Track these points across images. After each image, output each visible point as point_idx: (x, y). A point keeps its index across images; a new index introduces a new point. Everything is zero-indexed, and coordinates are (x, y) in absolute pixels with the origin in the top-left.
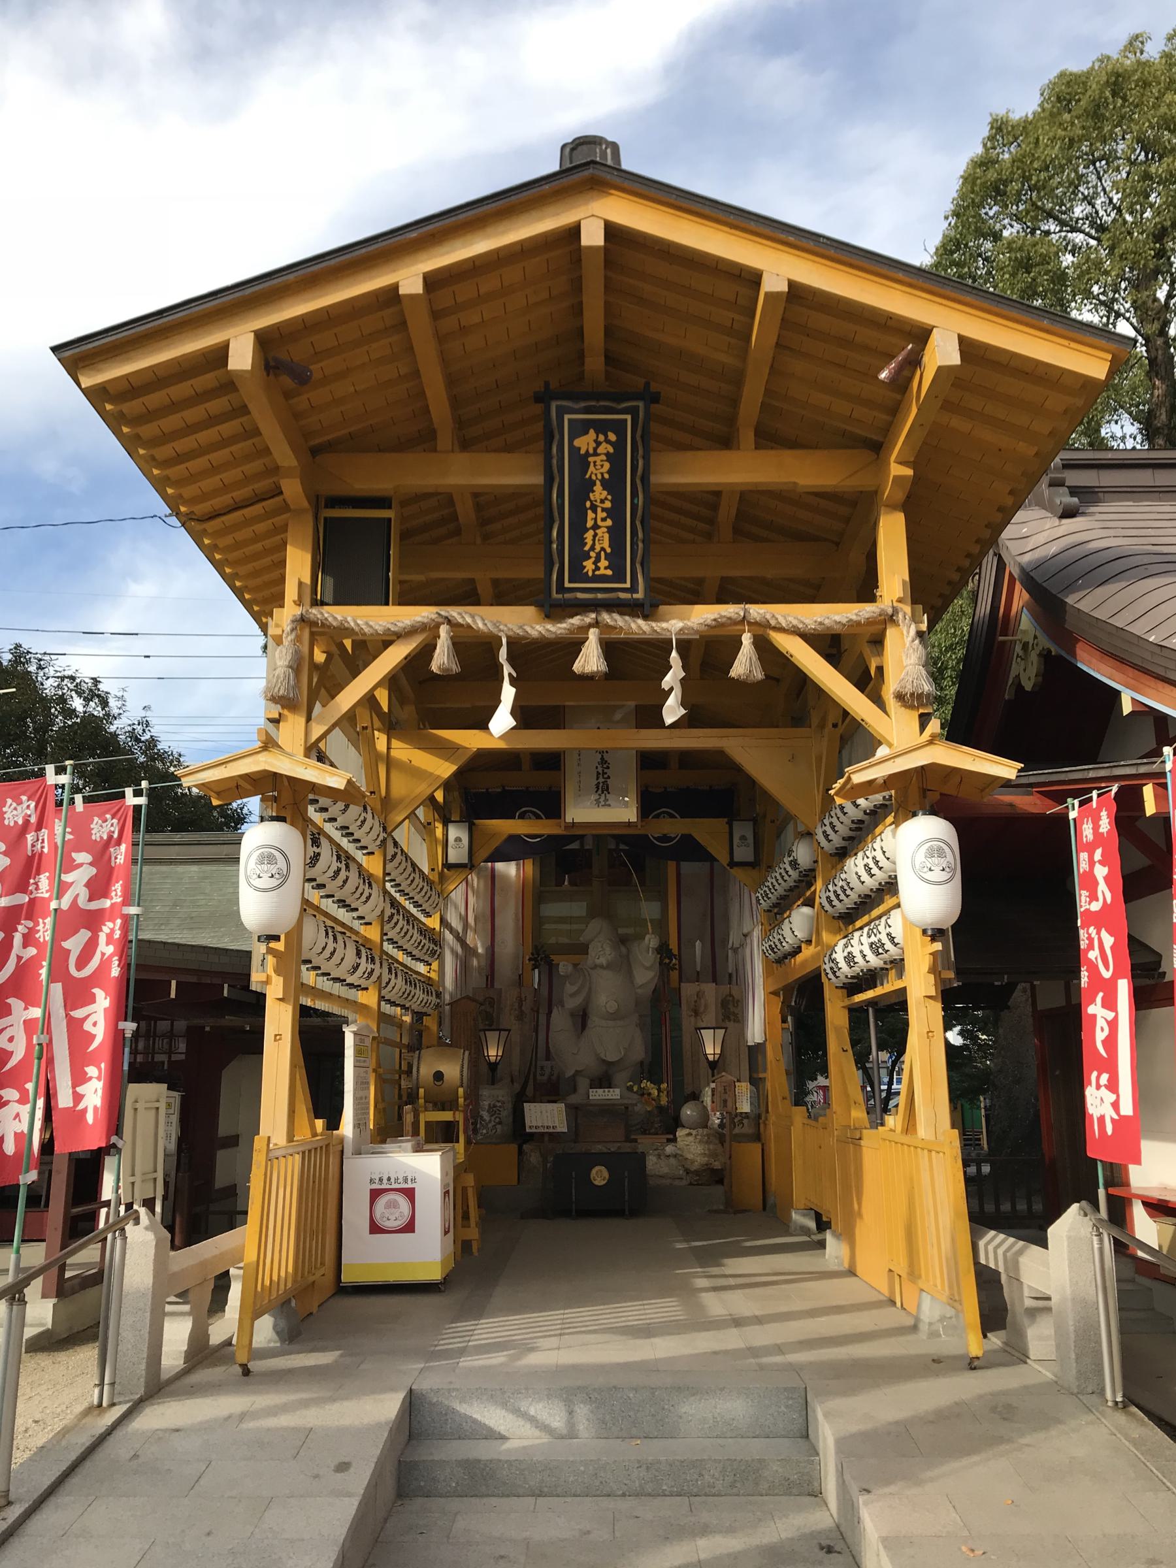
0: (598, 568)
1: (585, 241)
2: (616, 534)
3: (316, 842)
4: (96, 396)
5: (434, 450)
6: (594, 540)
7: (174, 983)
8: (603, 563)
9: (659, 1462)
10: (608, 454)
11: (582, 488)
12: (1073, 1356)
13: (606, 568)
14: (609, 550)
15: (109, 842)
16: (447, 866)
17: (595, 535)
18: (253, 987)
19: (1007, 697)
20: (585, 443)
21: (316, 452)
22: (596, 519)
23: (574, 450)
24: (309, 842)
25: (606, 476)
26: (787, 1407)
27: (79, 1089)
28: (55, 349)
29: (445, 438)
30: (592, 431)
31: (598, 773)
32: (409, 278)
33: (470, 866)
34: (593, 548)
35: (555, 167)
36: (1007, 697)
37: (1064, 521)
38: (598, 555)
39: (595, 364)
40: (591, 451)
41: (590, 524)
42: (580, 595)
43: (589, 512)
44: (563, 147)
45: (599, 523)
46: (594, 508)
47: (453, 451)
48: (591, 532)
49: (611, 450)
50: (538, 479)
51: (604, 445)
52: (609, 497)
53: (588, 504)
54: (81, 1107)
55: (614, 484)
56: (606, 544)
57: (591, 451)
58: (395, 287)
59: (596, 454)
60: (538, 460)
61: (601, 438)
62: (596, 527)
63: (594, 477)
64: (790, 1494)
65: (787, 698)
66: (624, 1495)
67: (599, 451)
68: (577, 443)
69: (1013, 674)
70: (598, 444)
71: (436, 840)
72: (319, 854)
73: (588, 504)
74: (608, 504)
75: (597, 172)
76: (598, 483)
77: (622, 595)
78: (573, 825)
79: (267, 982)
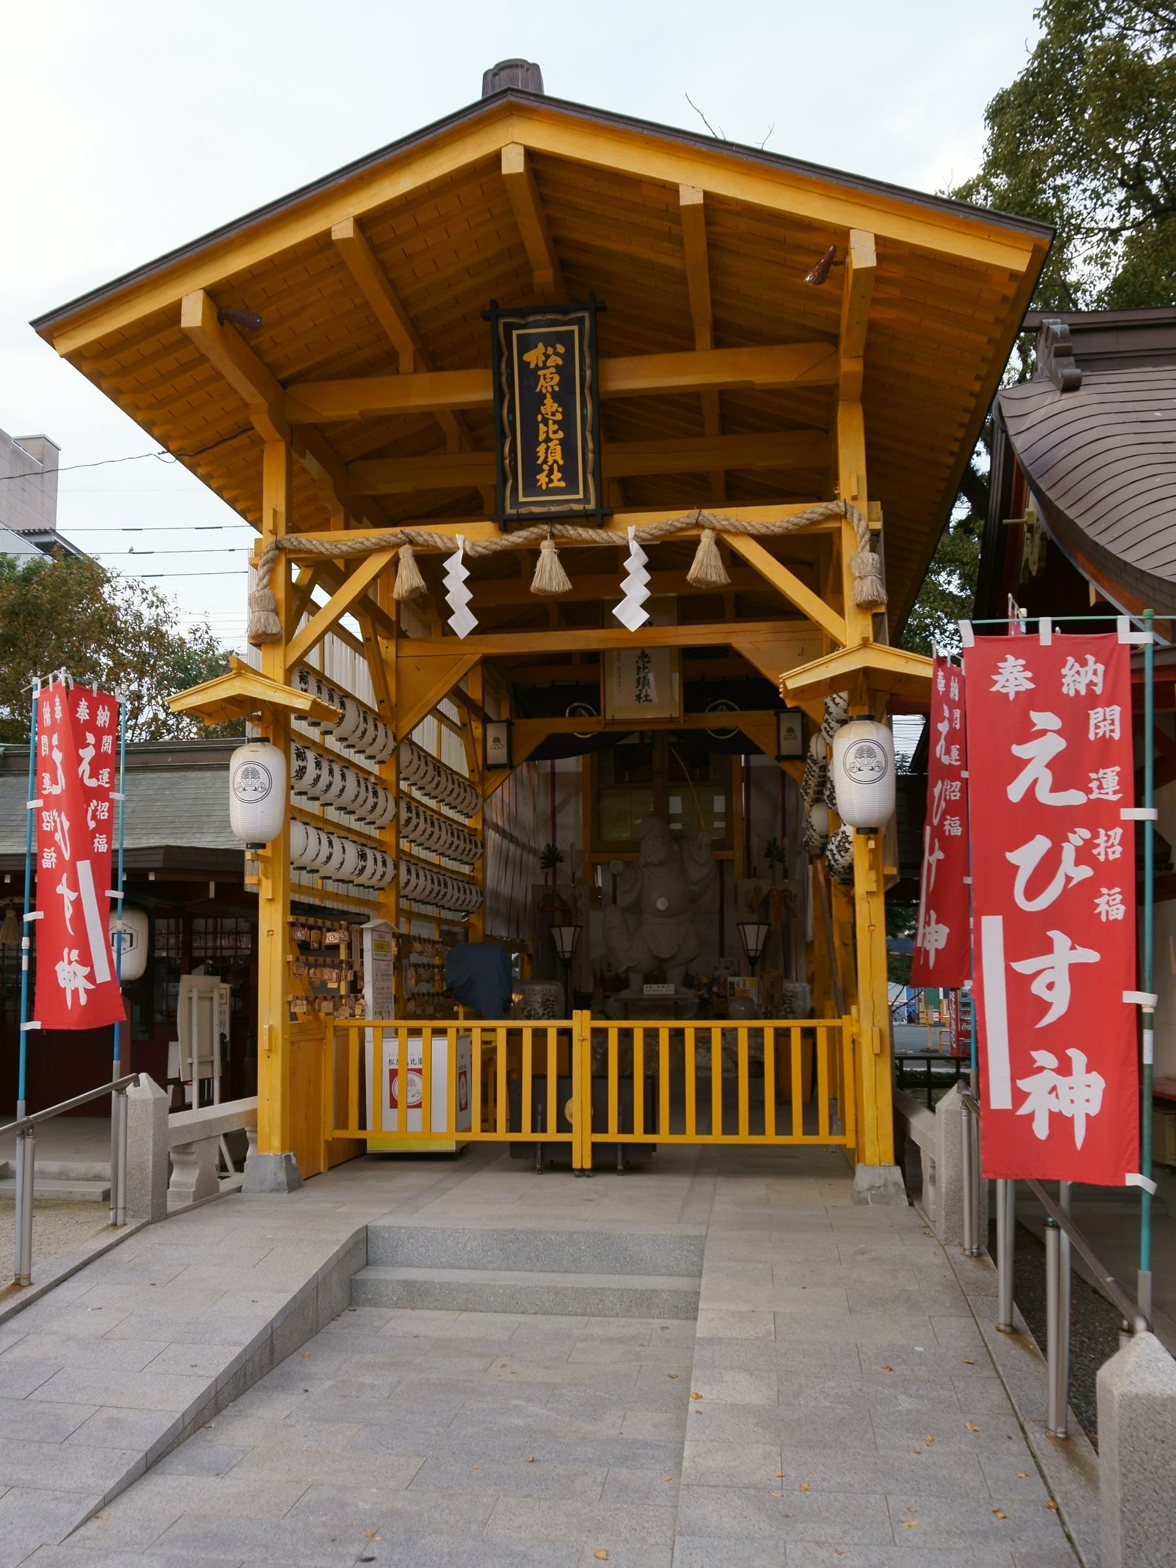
0: (551, 481)
1: (505, 170)
2: (568, 446)
3: (301, 756)
4: (76, 358)
5: (398, 372)
6: (546, 453)
7: (212, 885)
8: (557, 475)
9: (567, 1289)
10: (557, 367)
11: (533, 401)
12: (943, 1213)
13: (559, 480)
14: (561, 462)
15: (1092, 700)
16: (489, 768)
17: (548, 448)
18: (248, 889)
19: (1021, 581)
20: (533, 357)
21: (282, 383)
22: (547, 432)
23: (524, 366)
24: (294, 756)
25: (557, 389)
26: (689, 1251)
27: (1021, 1084)
28: (33, 324)
29: (406, 360)
30: (540, 345)
31: (639, 668)
32: (339, 222)
33: (510, 766)
34: (545, 461)
35: (478, 97)
36: (1021, 581)
37: (1066, 396)
38: (551, 467)
39: (544, 276)
40: (541, 365)
41: (542, 437)
42: (535, 510)
43: (541, 425)
44: (486, 75)
45: (551, 435)
46: (545, 421)
47: (415, 372)
48: (543, 446)
49: (560, 362)
50: (488, 395)
51: (553, 358)
52: (560, 409)
53: (539, 418)
54: (1023, 1111)
55: (564, 396)
56: (558, 456)
57: (541, 365)
58: (328, 232)
59: (545, 367)
60: (488, 375)
61: (550, 351)
62: (548, 440)
63: (544, 391)
64: (678, 1318)
65: (751, 599)
66: (536, 1313)
67: (548, 364)
68: (526, 357)
69: (1024, 559)
70: (547, 357)
71: (474, 740)
72: (305, 767)
73: (539, 418)
74: (559, 417)
75: (512, 99)
76: (548, 396)
77: (576, 507)
78: (614, 722)
79: (259, 884)
